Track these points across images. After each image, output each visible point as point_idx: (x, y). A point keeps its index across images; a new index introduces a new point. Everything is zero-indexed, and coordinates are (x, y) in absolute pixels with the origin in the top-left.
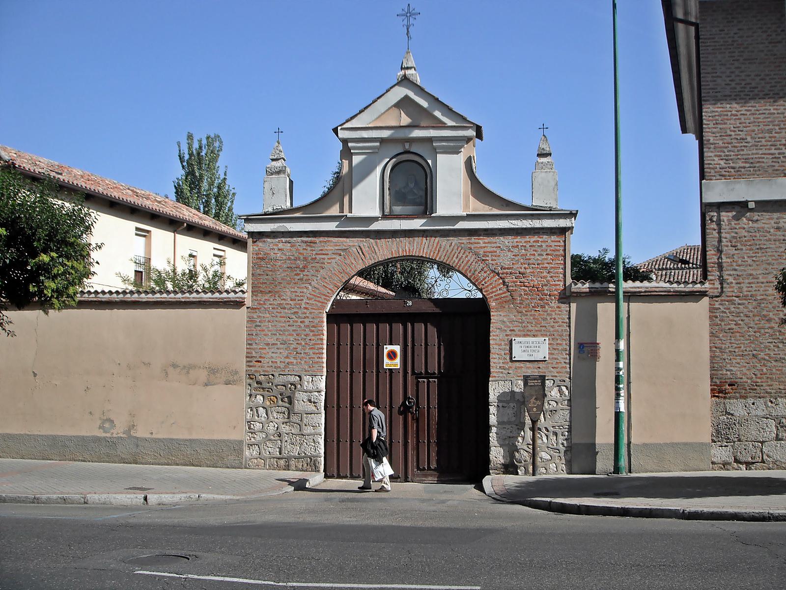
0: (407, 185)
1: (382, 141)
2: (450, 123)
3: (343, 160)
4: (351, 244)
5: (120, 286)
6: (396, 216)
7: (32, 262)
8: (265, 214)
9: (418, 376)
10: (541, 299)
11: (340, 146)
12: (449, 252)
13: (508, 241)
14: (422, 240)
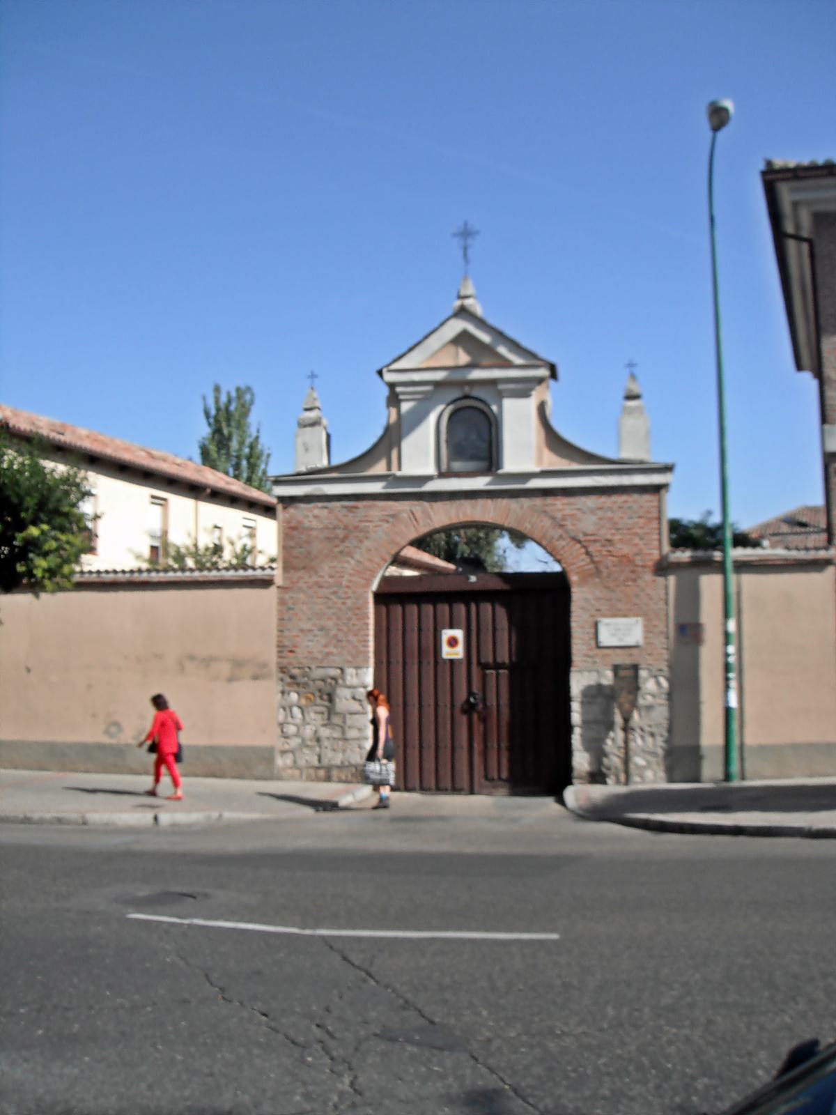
1: (437, 384)
2: (517, 360)
5: (129, 563)
7: (20, 536)
8: (298, 474)
9: (484, 666)
10: (633, 572)
11: (385, 391)
13: (590, 501)
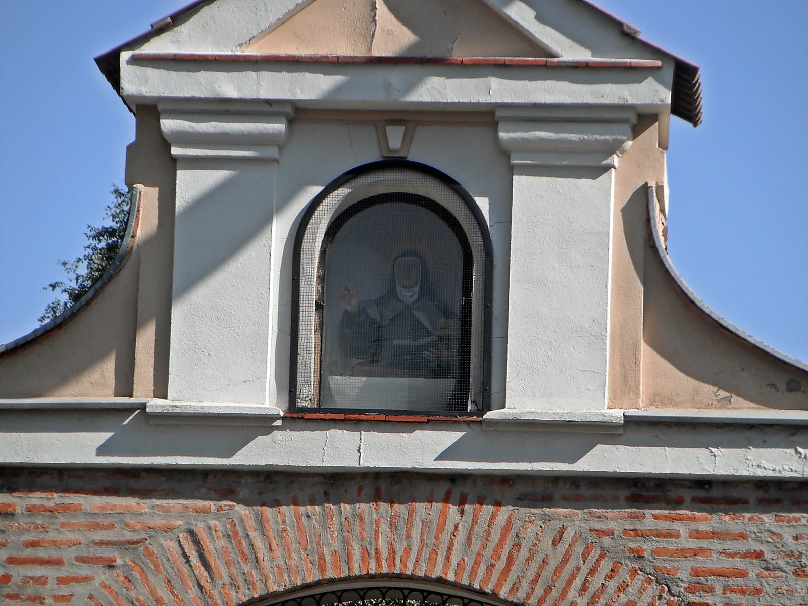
0: (392, 292)
1: (298, 114)
3: (140, 187)
4: (159, 522)
6: (342, 416)
12: (553, 563)
14: (443, 514)
